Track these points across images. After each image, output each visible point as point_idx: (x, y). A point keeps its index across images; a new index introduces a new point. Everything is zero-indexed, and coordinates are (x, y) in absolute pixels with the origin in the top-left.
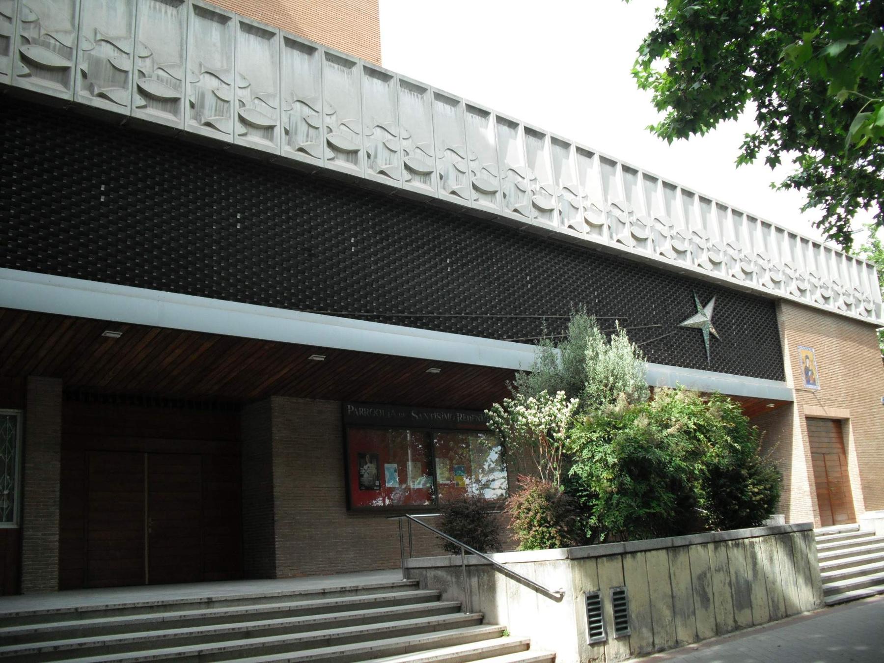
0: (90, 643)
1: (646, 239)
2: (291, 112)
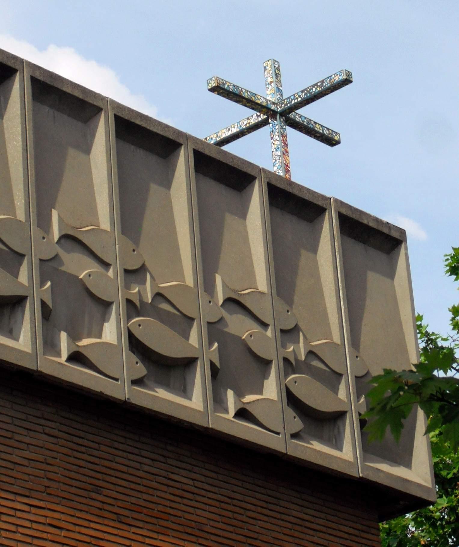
1: (340, 416)
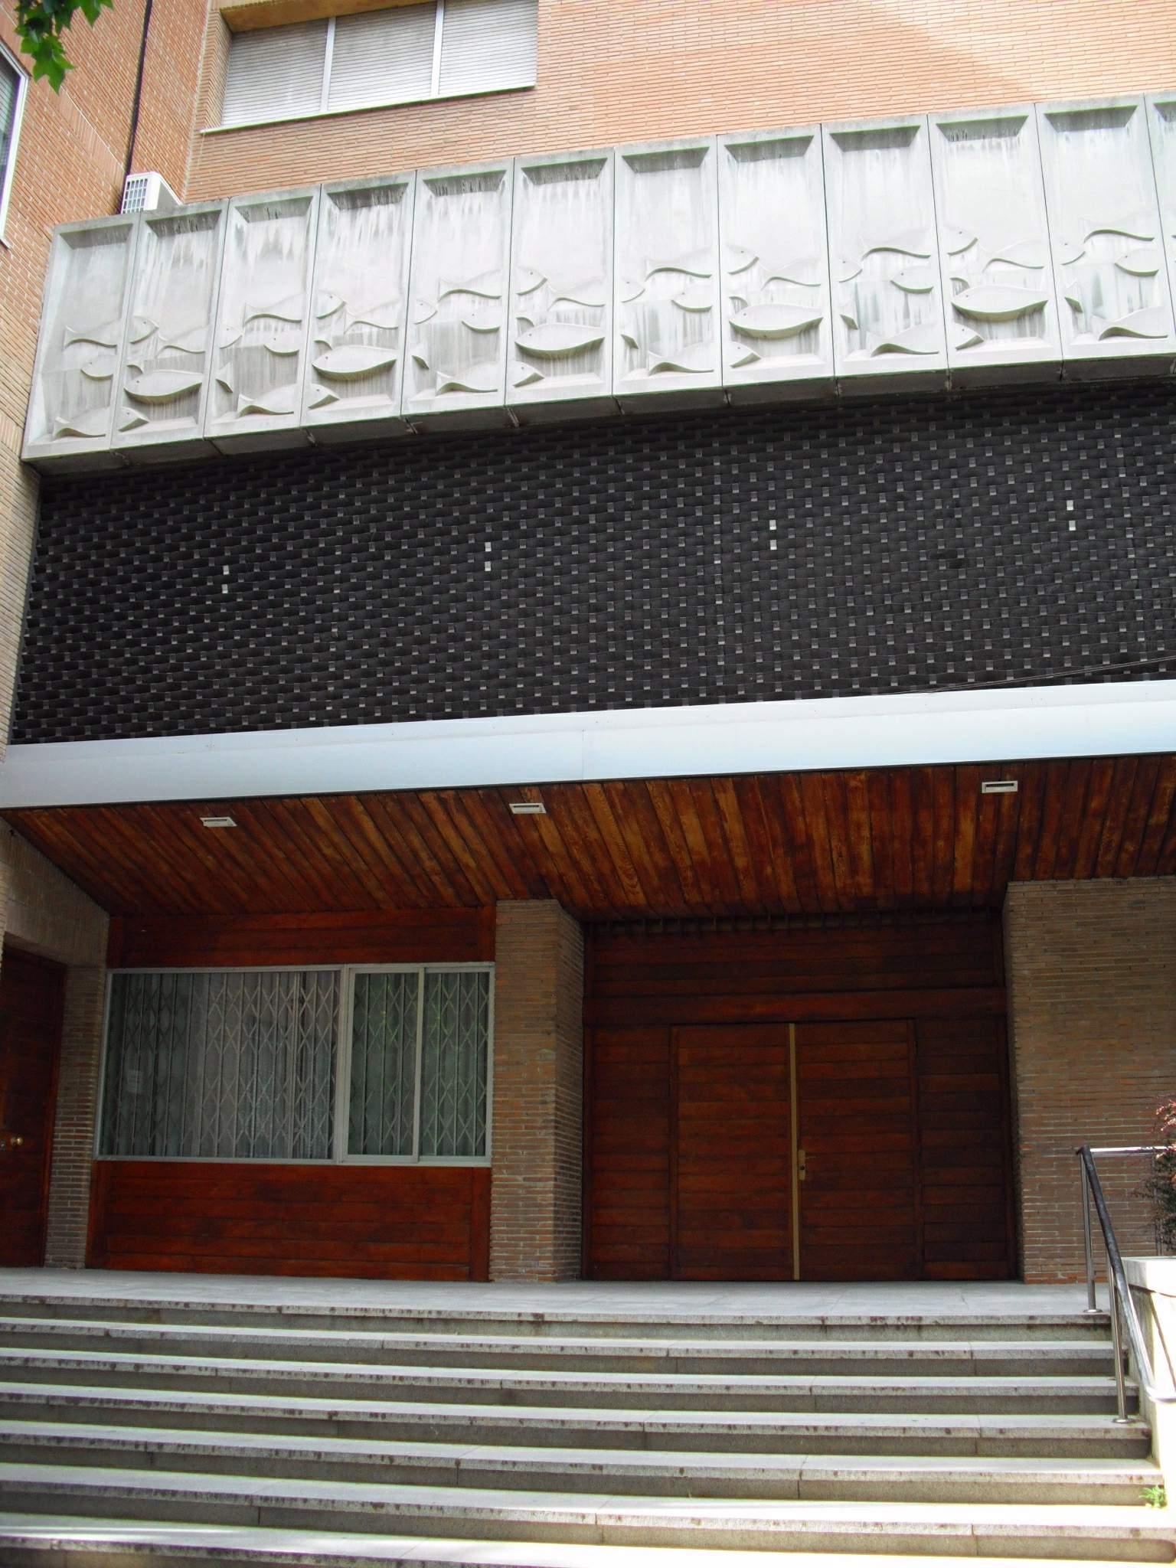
0: (194, 1367)
2: (858, 279)
